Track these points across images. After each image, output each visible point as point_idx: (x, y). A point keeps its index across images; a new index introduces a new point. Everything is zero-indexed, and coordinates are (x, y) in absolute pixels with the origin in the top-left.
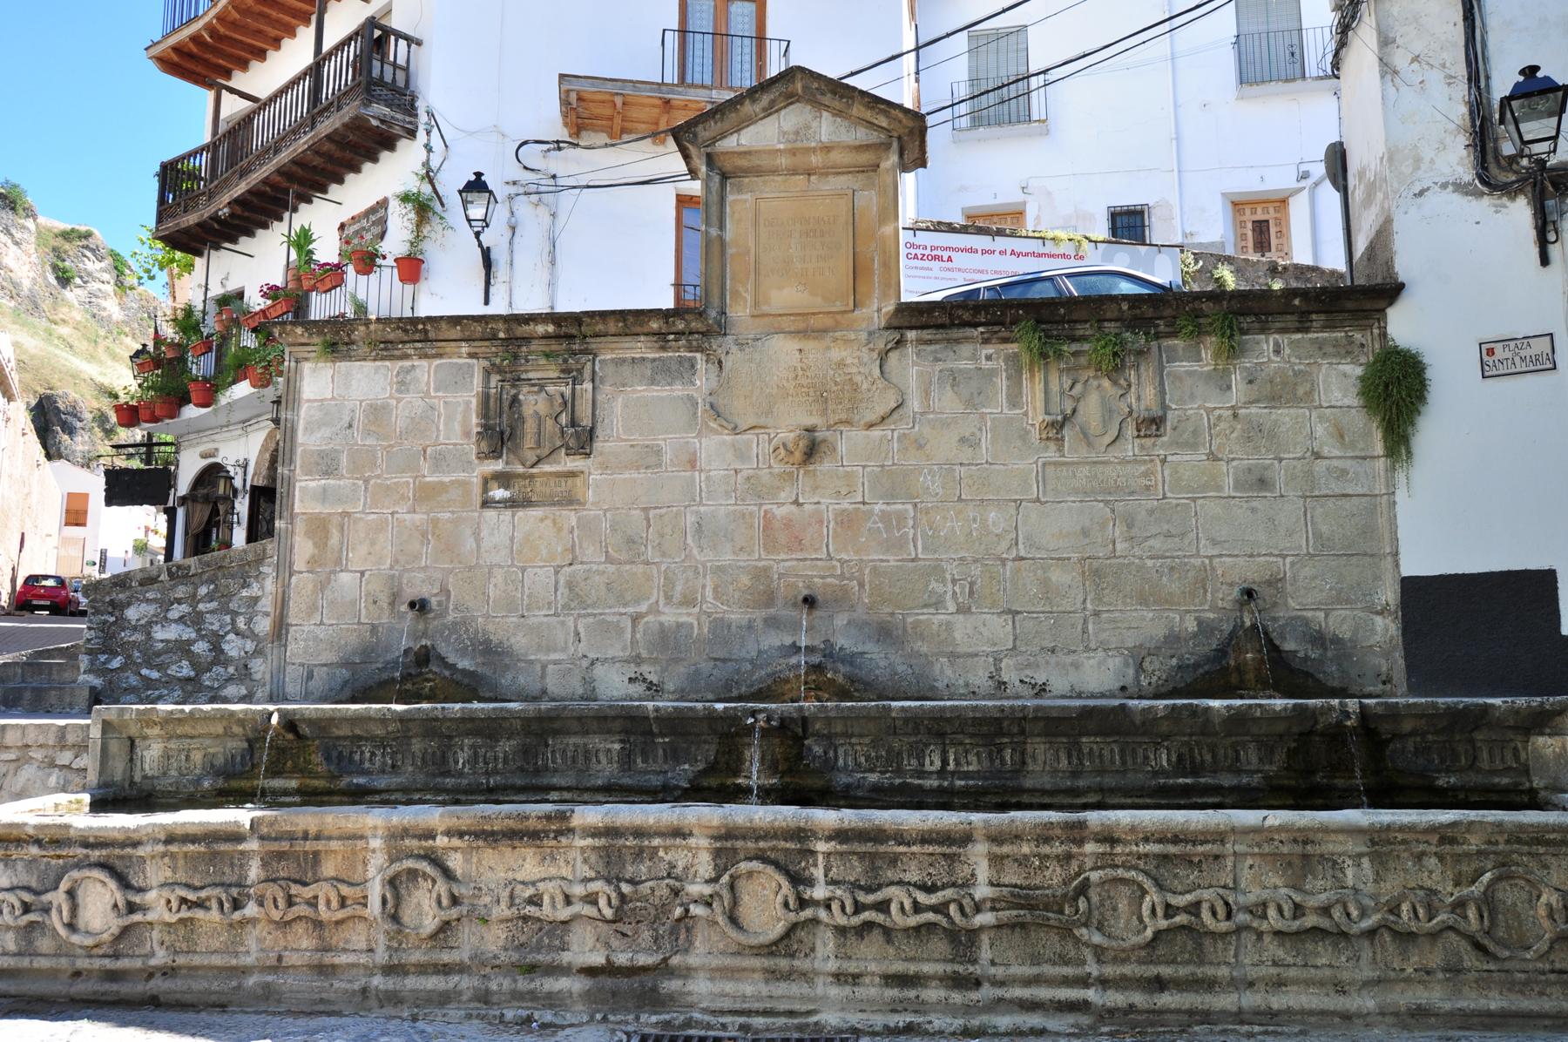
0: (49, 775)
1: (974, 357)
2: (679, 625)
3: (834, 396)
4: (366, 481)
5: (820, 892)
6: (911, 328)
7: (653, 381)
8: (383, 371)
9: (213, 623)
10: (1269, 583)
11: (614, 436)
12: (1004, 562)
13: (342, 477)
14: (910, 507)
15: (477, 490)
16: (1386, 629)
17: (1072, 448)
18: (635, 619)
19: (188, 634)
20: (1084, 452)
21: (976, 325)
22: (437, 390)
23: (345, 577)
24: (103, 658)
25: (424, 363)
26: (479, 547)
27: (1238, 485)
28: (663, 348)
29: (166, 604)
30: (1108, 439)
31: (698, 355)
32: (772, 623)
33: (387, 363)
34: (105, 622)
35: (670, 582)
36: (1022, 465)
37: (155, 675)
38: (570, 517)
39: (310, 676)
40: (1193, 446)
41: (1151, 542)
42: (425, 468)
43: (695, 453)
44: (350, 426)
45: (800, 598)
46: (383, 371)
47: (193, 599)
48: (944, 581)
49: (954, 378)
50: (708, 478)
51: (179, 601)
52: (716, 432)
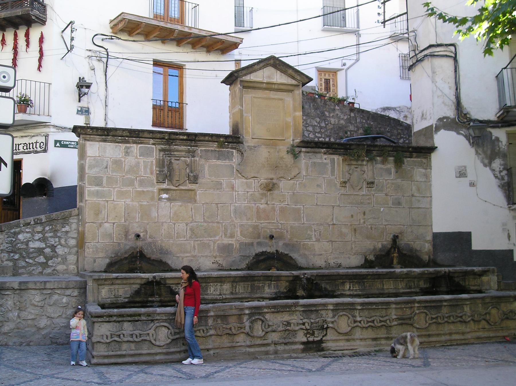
1: (321, 158)
2: (230, 244)
5: (359, 319)
6: (303, 147)
7: (218, 159)
9: (52, 241)
10: (400, 233)
11: (207, 176)
12: (329, 225)
13: (104, 187)
14: (302, 206)
15: (156, 194)
18: (214, 243)
21: (323, 148)
22: (140, 156)
24: (12, 254)
25: (135, 145)
27: (393, 204)
29: (33, 234)
30: (359, 188)
31: (234, 151)
32: (259, 244)
33: (120, 144)
34: (12, 240)
35: (226, 229)
37: (31, 261)
39: (95, 261)
40: (382, 191)
41: (369, 220)
42: (136, 184)
43: (233, 185)
44: (106, 168)
45: (268, 236)
47: (42, 232)
48: (312, 231)
50: (238, 194)
52: (240, 178)
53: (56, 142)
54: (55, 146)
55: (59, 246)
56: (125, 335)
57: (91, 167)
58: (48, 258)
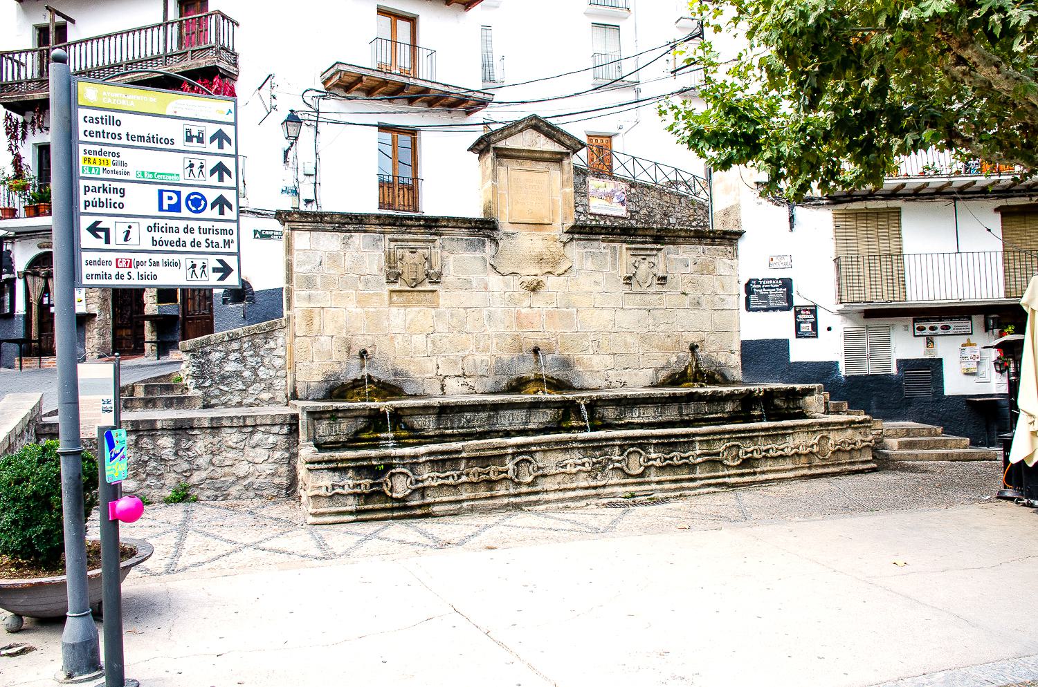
1: (598, 248)
3: (549, 262)
11: (450, 276)
16: (736, 359)
17: (635, 288)
19: (240, 367)
20: (639, 289)
21: (602, 234)
23: (322, 339)
24: (201, 381)
27: (691, 304)
28: (471, 235)
35: (478, 341)
37: (226, 389)
38: (433, 312)
41: (662, 326)
42: (361, 286)
43: (486, 284)
49: (593, 255)
51: (234, 351)
55: (262, 368)
57: (301, 263)
58: (248, 384)
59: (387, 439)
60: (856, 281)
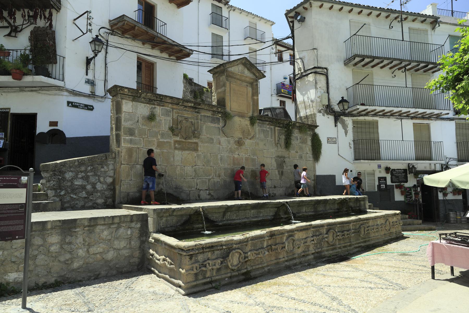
0: (128, 230)
2: (218, 182)
4: (143, 139)
7: (212, 122)
8: (147, 107)
9: (92, 179)
11: (205, 135)
13: (136, 137)
18: (209, 181)
22: (162, 115)
24: (58, 191)
25: (158, 107)
26: (174, 160)
27: (299, 158)
36: (272, 150)
37: (75, 197)
38: (195, 154)
44: (138, 122)
46: (147, 107)
49: (263, 131)
51: (81, 172)
53: (68, 103)
54: (68, 105)
56: (211, 265)
59: (327, 250)
60: (361, 151)
